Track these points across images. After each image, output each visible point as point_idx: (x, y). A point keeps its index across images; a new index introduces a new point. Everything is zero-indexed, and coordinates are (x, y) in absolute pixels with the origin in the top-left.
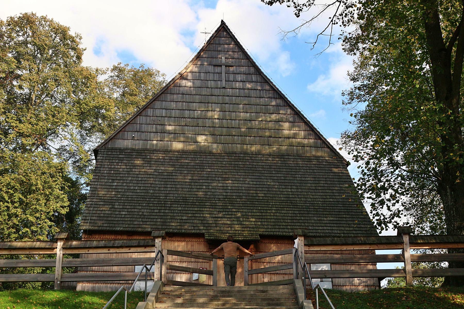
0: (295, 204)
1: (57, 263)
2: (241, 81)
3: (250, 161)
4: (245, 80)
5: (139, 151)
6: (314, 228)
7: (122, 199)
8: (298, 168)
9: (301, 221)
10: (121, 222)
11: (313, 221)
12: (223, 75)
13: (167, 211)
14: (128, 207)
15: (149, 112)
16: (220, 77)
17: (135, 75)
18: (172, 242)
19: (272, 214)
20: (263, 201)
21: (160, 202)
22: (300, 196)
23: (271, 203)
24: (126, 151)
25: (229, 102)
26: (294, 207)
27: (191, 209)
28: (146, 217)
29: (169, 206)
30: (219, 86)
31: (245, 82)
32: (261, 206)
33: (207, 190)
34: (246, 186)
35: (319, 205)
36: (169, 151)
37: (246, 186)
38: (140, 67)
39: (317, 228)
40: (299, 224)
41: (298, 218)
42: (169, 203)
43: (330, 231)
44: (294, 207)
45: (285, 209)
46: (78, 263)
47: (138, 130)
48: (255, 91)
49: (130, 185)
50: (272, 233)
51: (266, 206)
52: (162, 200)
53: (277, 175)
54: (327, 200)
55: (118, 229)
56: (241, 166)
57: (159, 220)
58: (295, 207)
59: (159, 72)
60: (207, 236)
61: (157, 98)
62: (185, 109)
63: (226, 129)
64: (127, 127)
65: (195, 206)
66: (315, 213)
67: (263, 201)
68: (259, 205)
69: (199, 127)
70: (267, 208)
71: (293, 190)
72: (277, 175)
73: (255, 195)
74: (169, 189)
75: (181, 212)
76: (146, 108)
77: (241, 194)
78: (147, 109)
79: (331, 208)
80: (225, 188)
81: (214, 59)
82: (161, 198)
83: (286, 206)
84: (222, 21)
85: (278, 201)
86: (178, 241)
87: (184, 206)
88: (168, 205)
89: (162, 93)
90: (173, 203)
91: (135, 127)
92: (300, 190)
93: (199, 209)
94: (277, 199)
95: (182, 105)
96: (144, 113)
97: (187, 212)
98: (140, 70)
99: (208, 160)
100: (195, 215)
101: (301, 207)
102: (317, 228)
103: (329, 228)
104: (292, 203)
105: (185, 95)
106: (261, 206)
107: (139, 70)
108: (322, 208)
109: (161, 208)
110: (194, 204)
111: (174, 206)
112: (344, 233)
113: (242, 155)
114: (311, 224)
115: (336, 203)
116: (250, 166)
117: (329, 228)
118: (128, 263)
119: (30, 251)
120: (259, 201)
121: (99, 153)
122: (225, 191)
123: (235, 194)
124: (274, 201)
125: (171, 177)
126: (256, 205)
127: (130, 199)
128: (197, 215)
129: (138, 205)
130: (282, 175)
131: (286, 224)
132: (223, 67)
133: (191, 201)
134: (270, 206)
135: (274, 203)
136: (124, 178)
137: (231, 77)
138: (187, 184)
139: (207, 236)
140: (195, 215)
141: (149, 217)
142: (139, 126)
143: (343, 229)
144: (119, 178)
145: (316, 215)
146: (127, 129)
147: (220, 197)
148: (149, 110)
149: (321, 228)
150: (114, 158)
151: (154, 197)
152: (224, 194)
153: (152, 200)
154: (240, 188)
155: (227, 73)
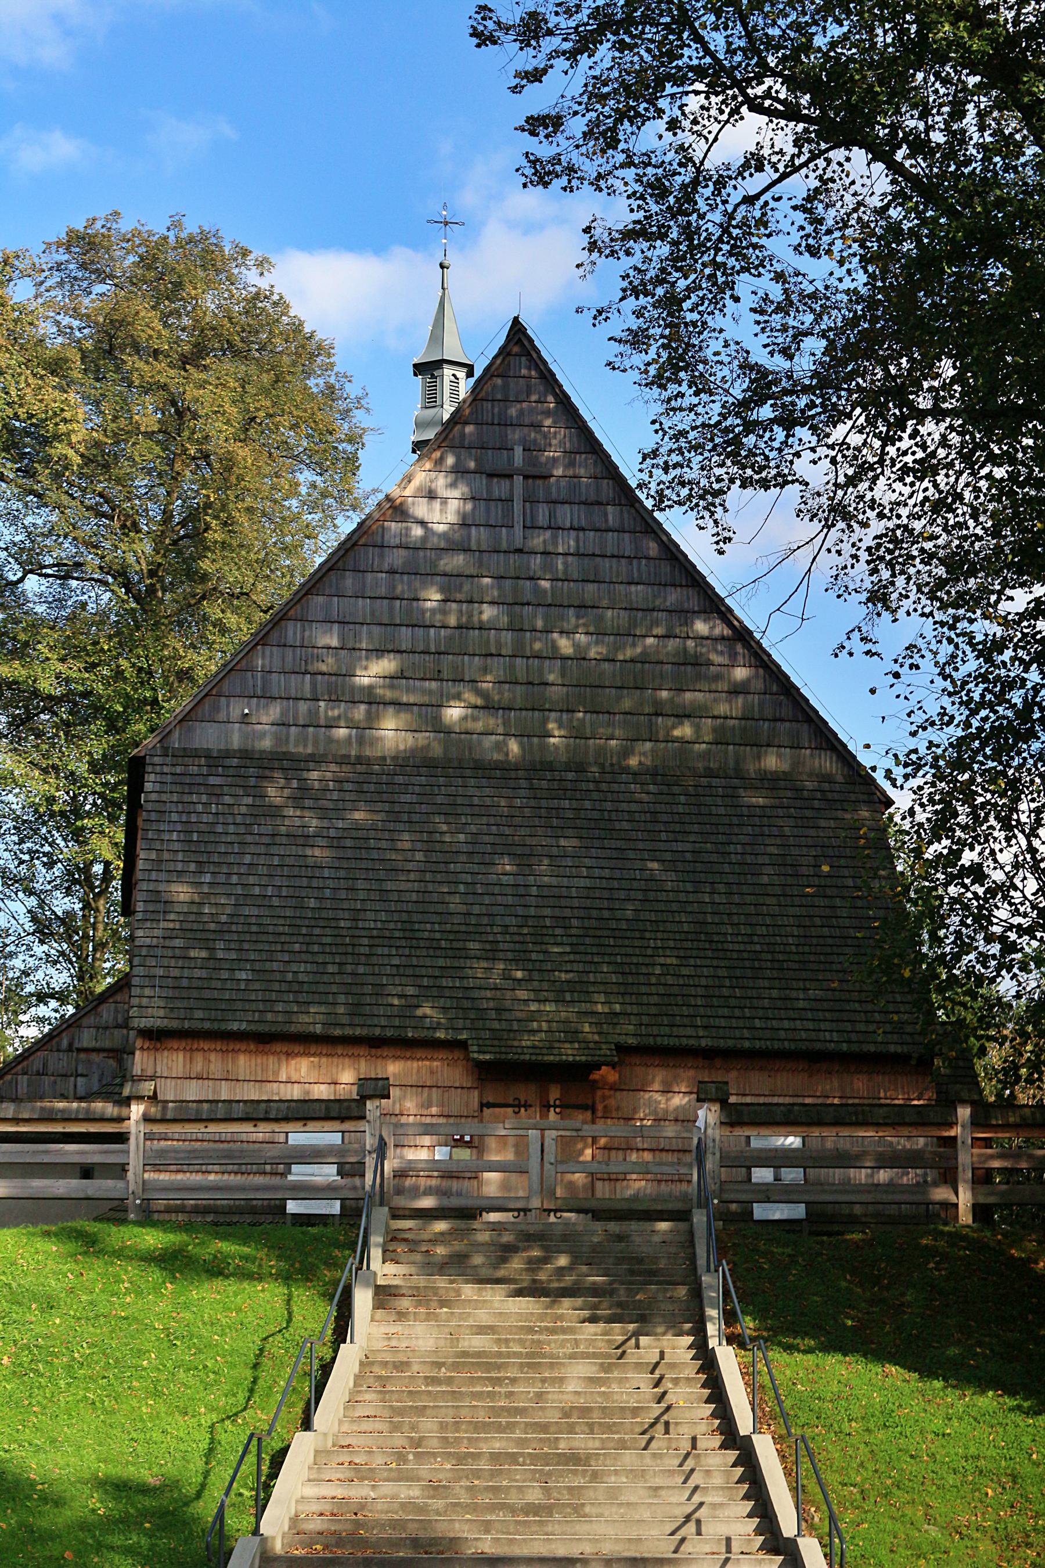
0: (720, 946)
1: (132, 1155)
2: (572, 528)
3: (595, 795)
4: (583, 524)
5: (266, 762)
6: (769, 1024)
7: (234, 928)
8: (735, 820)
9: (733, 1002)
10: (239, 1005)
11: (766, 1003)
12: (518, 506)
13: (361, 969)
14: (252, 956)
15: (290, 633)
16: (509, 512)
17: (147, 262)
18: (379, 1061)
19: (653, 980)
20: (628, 934)
21: (339, 940)
22: (735, 919)
23: (652, 943)
24: (228, 762)
25: (534, 601)
26: (716, 954)
27: (428, 962)
28: (306, 987)
29: (366, 951)
30: (504, 546)
31: (583, 529)
32: (623, 951)
33: (470, 899)
34: (582, 882)
35: (788, 949)
36: (353, 761)
37: (582, 882)
38: (169, 229)
39: (775, 1024)
40: (726, 1012)
41: (726, 992)
42: (366, 941)
43: (813, 1035)
44: (716, 954)
45: (692, 962)
46: (182, 1155)
47: (259, 693)
48: (614, 560)
49: (252, 880)
50: (651, 1040)
51: (637, 951)
52: (344, 932)
53: (674, 846)
54: (814, 932)
55: (235, 1026)
56: (570, 814)
57: (342, 999)
58: (721, 954)
59: (245, 253)
60: (475, 1048)
61: (313, 586)
62: (398, 622)
63: (524, 687)
64: (226, 681)
65: (438, 953)
66: (775, 974)
67: (628, 934)
68: (617, 950)
69: (442, 680)
70: (641, 960)
71: (717, 899)
72: (674, 846)
73: (606, 914)
74: (362, 895)
75: (402, 971)
76: (281, 619)
77: (567, 913)
78: (283, 623)
79: (822, 958)
80: (522, 891)
81: (490, 452)
82: (342, 924)
83: (695, 953)
84: (516, 320)
85: (671, 936)
86: (396, 1058)
87: (407, 951)
88: (362, 950)
89: (330, 569)
90: (376, 941)
91: (251, 683)
92: (736, 899)
93: (449, 962)
94: (669, 926)
95: (391, 609)
96: (274, 636)
97: (418, 971)
98: (172, 239)
99: (471, 791)
100: (438, 982)
101: (735, 955)
102: (775, 1024)
103: (810, 1025)
104: (711, 942)
105: (397, 576)
106: (623, 951)
107: (165, 238)
108: (796, 958)
109: (343, 959)
110: (435, 944)
111: (379, 950)
112: (849, 1042)
113: (571, 776)
114: (761, 1013)
115: (838, 942)
116: (596, 815)
117: (810, 1025)
118: (301, 1157)
119: (63, 1124)
120: (617, 933)
121: (149, 769)
122: (522, 901)
123: (548, 912)
124: (659, 935)
125: (364, 854)
126: (609, 950)
127: (254, 929)
128: (444, 982)
129: (279, 947)
130: (689, 847)
131: (692, 1011)
132: (518, 480)
133: (426, 935)
134: (649, 952)
135: (659, 943)
136: (231, 859)
137: (542, 514)
138: (412, 876)
139: (475, 1048)
140: (438, 982)
141: (314, 988)
142: (263, 677)
143: (848, 1026)
144: (216, 858)
145: (776, 983)
146: (226, 687)
147: (508, 920)
148: (290, 625)
149: (786, 1024)
150: (195, 789)
151: (322, 923)
152: (520, 911)
153: (317, 931)
154: (564, 892)
155: (530, 500)
